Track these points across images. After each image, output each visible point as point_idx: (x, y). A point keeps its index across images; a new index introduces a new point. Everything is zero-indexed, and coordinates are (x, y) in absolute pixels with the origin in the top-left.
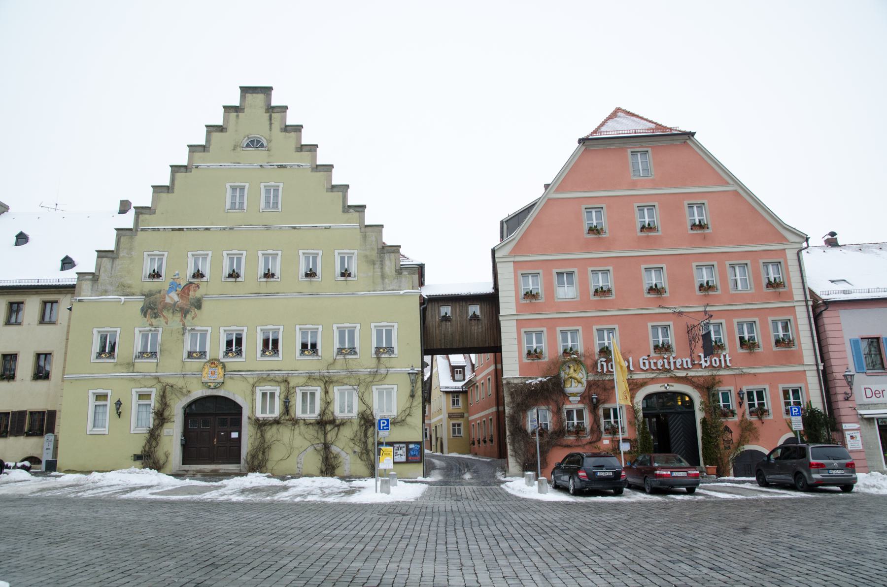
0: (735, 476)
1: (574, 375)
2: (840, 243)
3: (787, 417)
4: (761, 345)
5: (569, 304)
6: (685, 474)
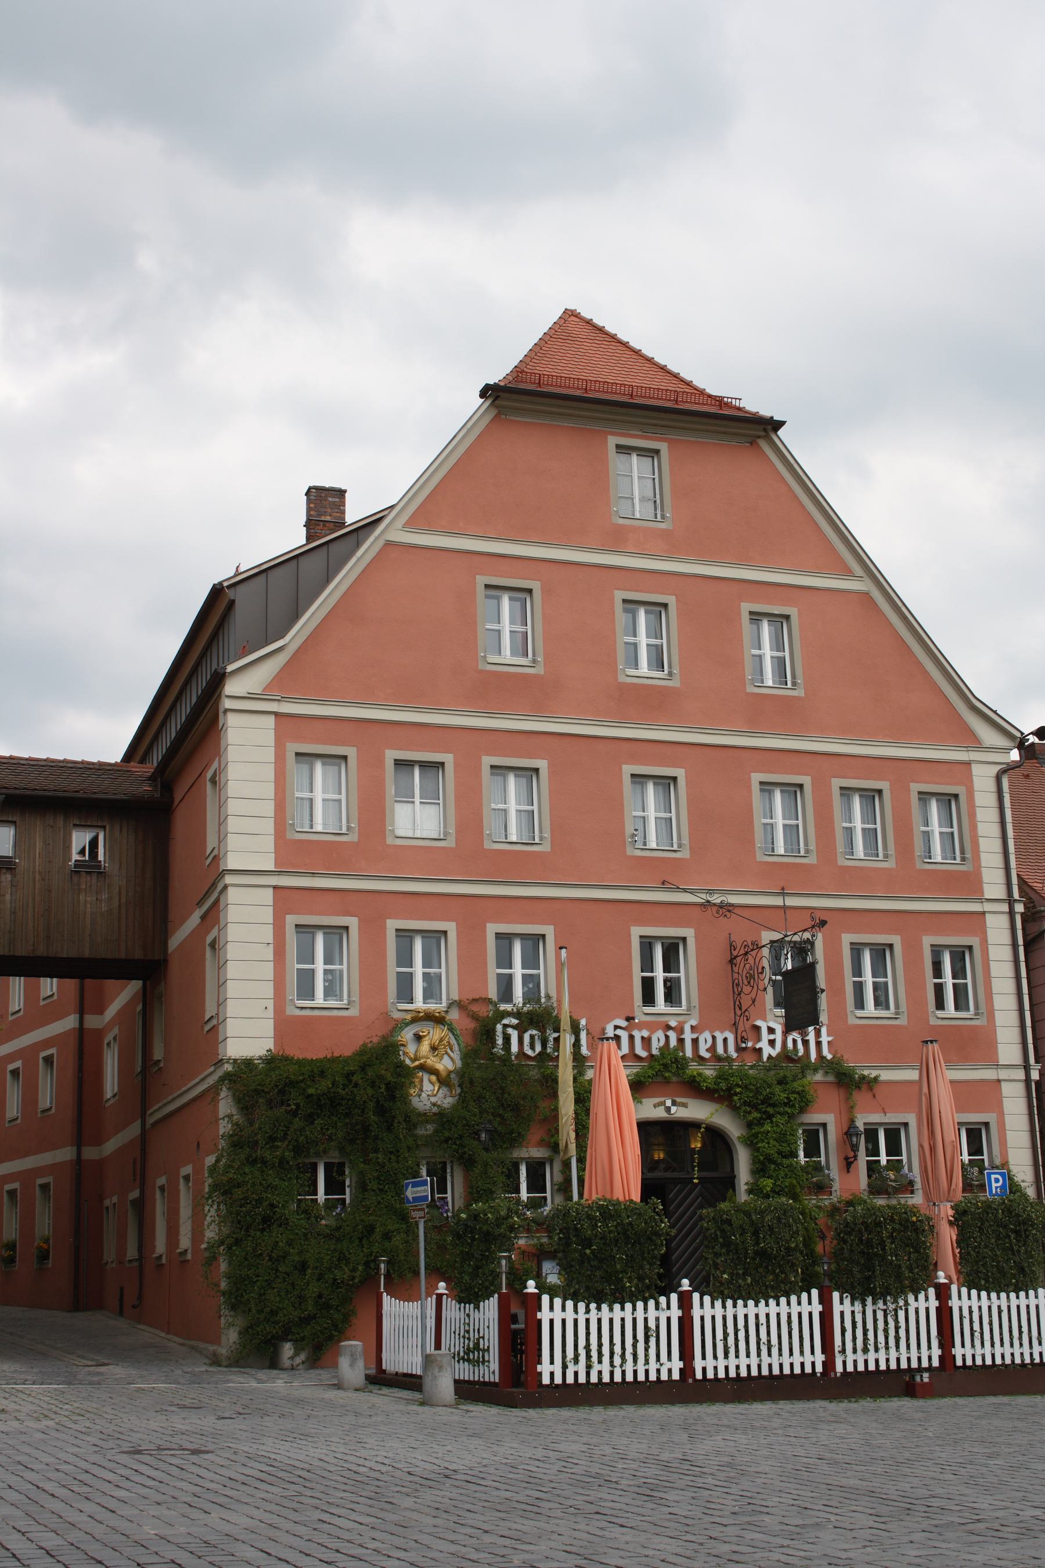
5: (420, 857)
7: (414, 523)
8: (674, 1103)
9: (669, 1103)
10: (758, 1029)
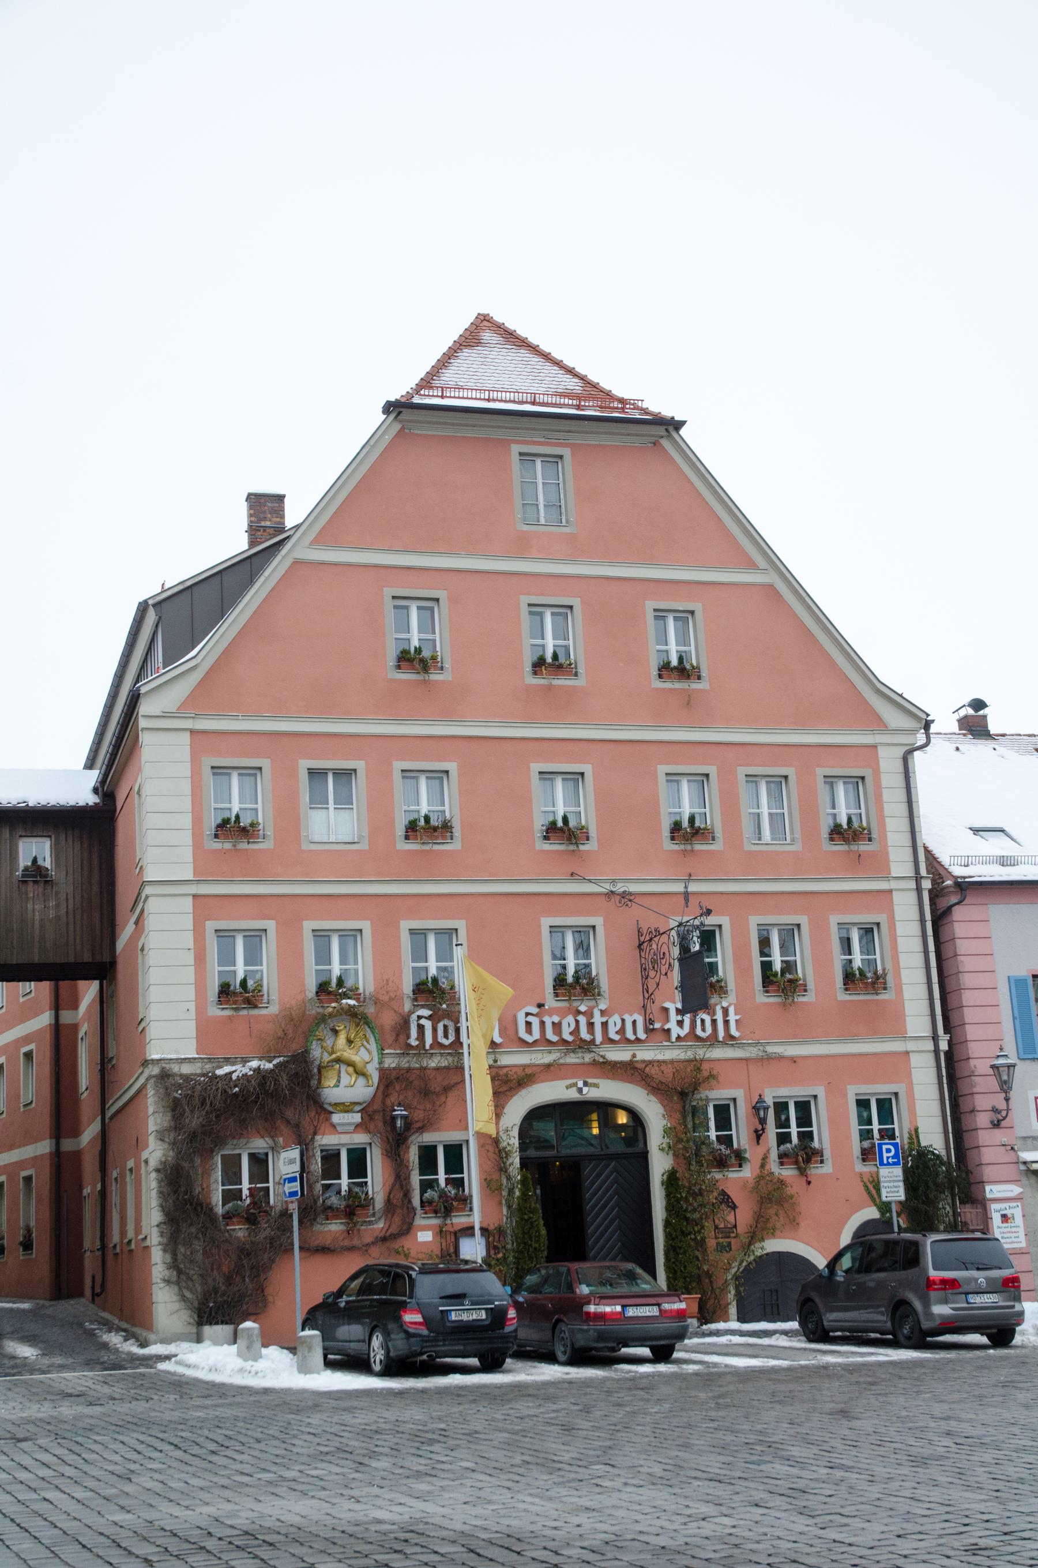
0: (741, 1319)
1: (349, 1054)
2: (993, 729)
3: (867, 1169)
4: (811, 985)
5: (339, 859)
6: (654, 1311)
7: (319, 541)
8: (586, 1084)
9: (580, 1084)
10: (666, 1010)
